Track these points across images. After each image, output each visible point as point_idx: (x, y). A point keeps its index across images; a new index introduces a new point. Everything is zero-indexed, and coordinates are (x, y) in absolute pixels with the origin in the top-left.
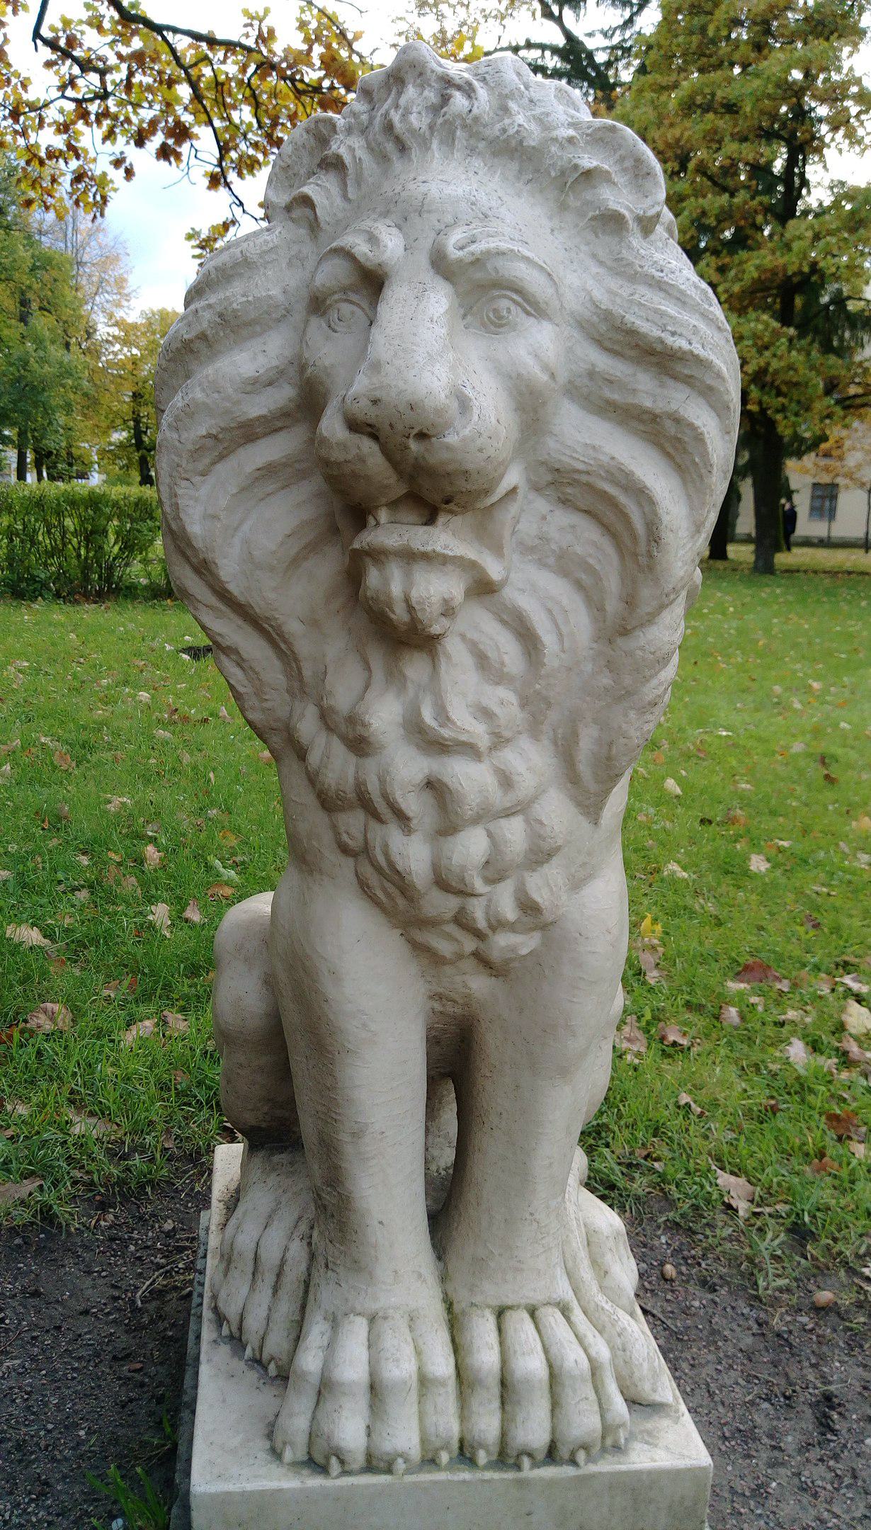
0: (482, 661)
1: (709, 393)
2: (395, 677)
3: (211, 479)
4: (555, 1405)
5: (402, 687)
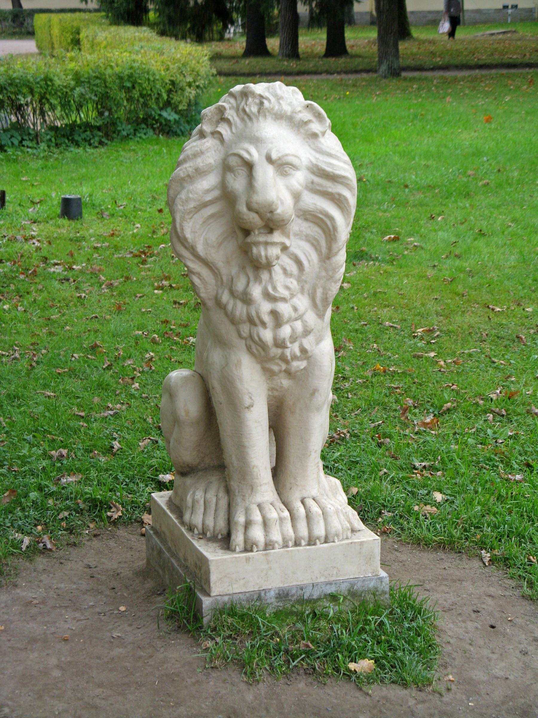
0: (285, 271)
1: (348, 186)
2: (258, 279)
3: (193, 220)
4: (325, 520)
5: (260, 282)
